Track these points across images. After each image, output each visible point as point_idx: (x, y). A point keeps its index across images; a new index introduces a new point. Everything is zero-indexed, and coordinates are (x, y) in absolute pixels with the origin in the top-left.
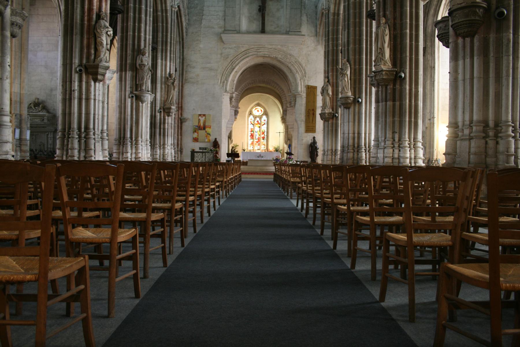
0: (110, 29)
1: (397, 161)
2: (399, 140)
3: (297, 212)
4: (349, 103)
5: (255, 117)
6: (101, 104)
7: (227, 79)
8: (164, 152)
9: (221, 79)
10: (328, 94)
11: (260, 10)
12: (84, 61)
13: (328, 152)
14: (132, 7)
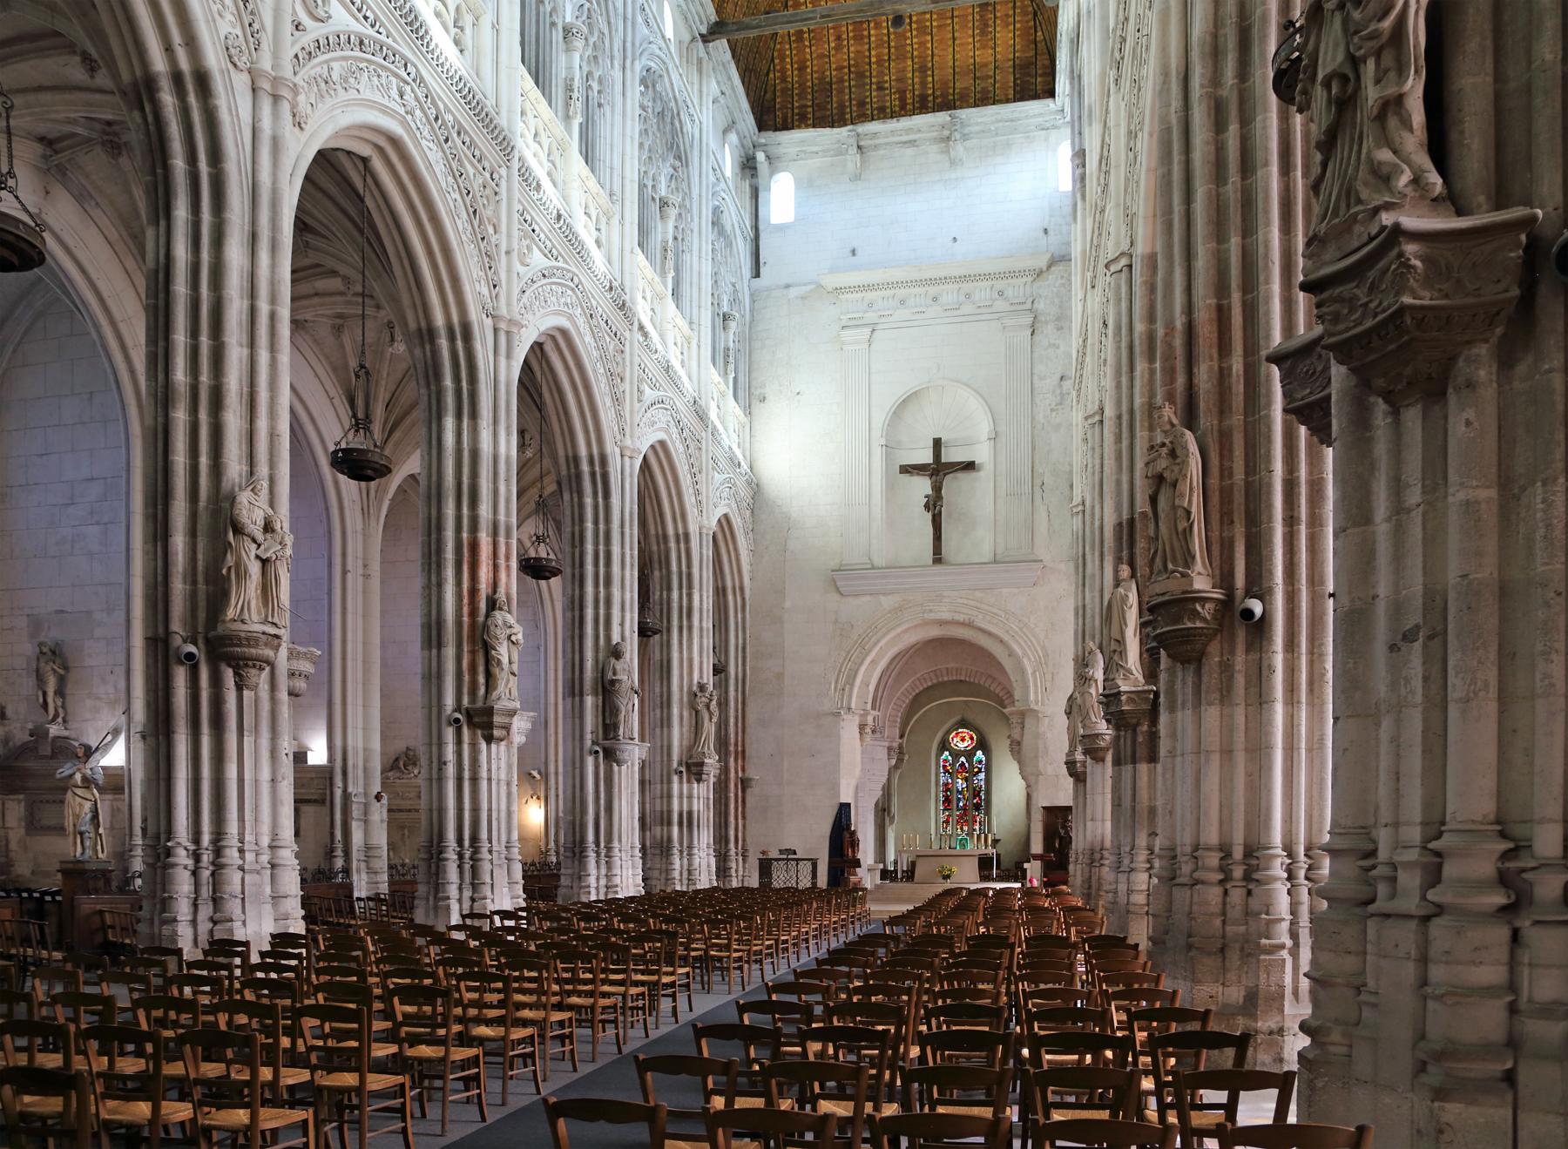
6: (504, 788)
7: (851, 681)
8: (690, 865)
11: (927, 507)
12: (465, 701)
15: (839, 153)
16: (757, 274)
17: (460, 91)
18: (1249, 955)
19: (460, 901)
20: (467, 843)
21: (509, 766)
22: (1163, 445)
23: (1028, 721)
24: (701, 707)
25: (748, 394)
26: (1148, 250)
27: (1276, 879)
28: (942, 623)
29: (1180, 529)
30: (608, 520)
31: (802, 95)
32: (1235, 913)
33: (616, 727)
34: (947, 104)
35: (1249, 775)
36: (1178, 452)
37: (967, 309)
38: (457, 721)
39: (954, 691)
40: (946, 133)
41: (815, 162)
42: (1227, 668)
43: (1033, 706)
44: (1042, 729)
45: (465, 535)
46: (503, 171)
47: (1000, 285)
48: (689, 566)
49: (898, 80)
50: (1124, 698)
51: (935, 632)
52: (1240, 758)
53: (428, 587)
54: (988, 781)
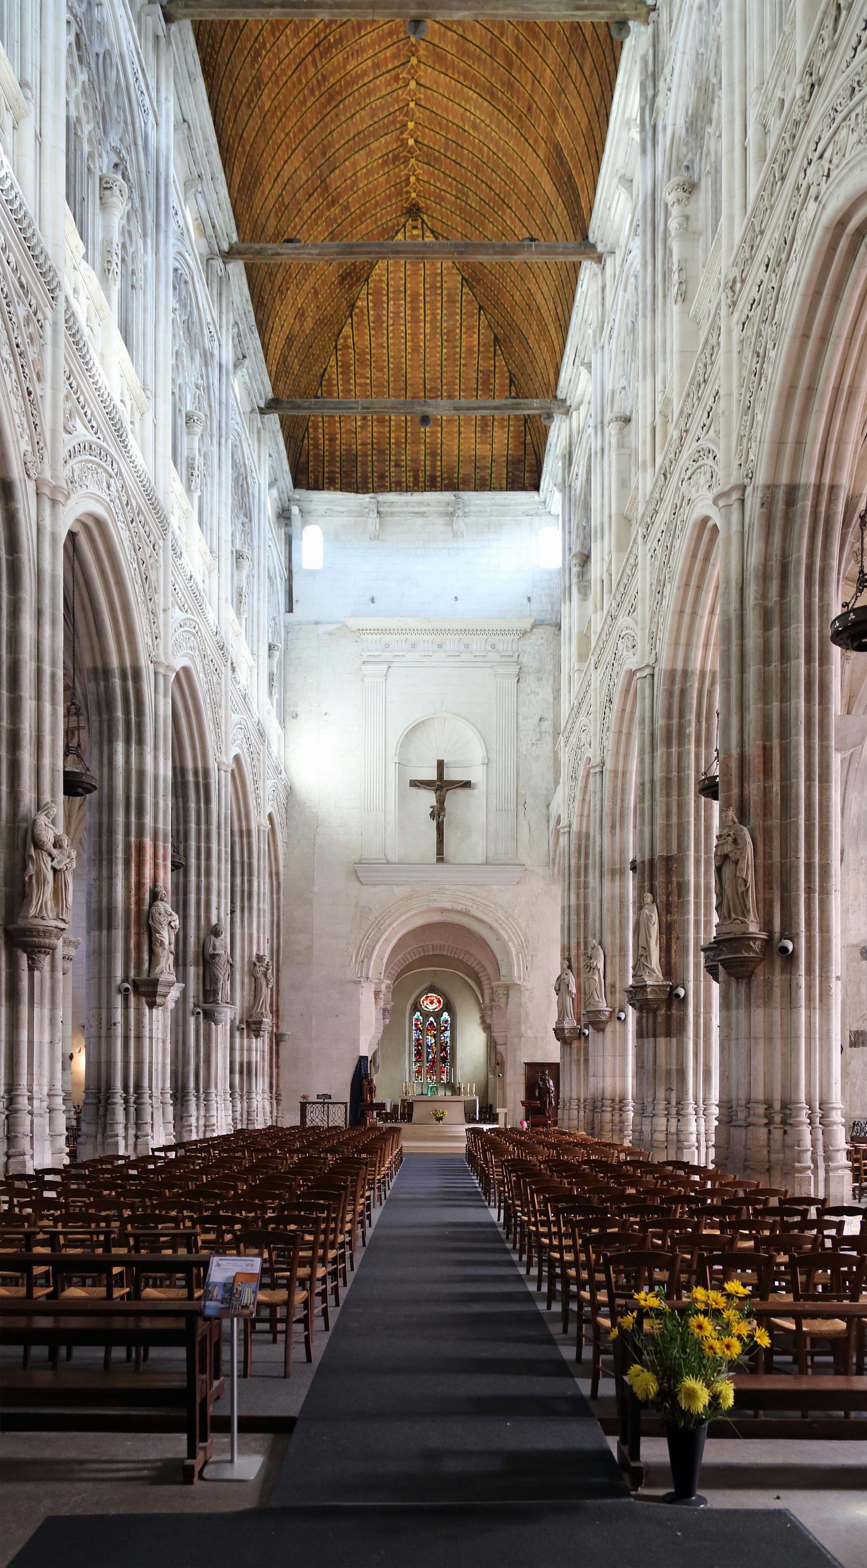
0: (176, 917)
1: (675, 1137)
2: (678, 1103)
3: (494, 1229)
4: (603, 1022)
6: (160, 1045)
7: (369, 956)
8: (249, 1107)
9: (357, 956)
10: (570, 993)
11: (432, 815)
15: (361, 515)
16: (290, 610)
17: (141, 482)
18: (787, 1174)
19: (126, 1138)
20: (131, 1090)
21: (165, 1027)
22: (729, 835)
23: (512, 994)
24: (259, 975)
25: (286, 714)
26: (669, 668)
27: (802, 1123)
28: (443, 910)
29: (740, 891)
30: (208, 822)
31: (331, 462)
32: (777, 1144)
34: (452, 486)
35: (783, 1054)
36: (739, 841)
37: (466, 657)
38: (127, 990)
39: (448, 963)
40: (451, 509)
41: (341, 520)
42: (768, 984)
44: (523, 1000)
45: (133, 839)
46: (161, 542)
47: (493, 639)
48: (250, 857)
49: (413, 461)
50: (649, 990)
51: (437, 918)
52: (778, 1043)
53: (99, 878)
54: (453, 1038)
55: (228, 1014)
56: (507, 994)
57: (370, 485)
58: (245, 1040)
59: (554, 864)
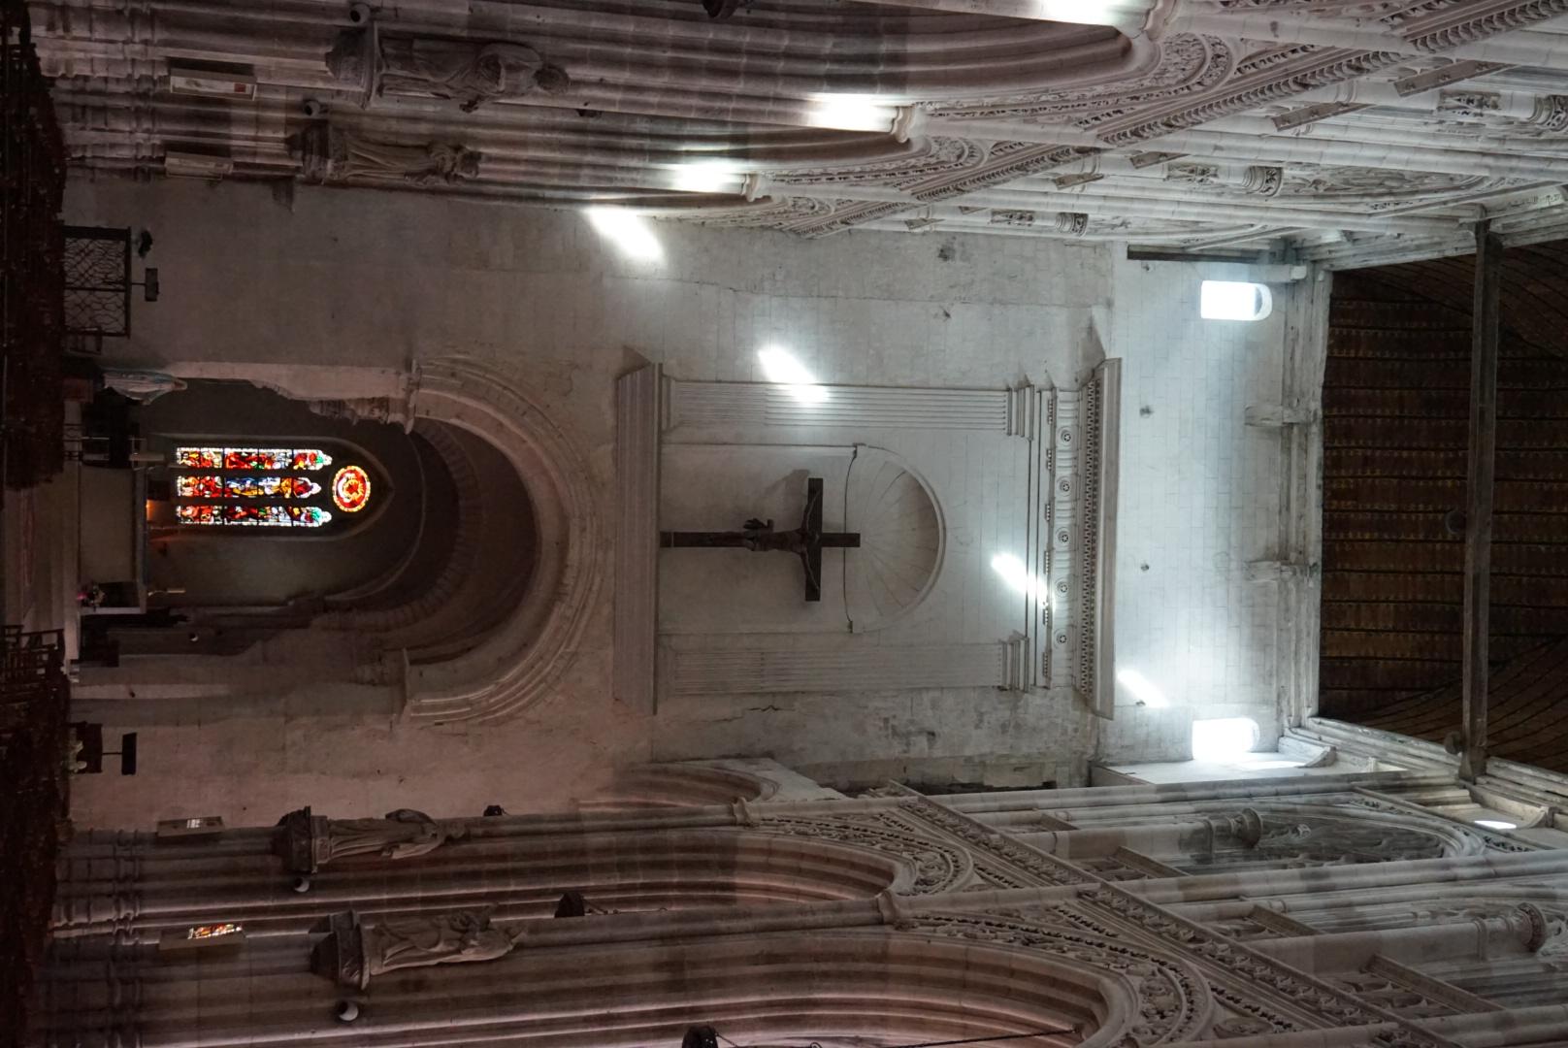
4: (335, 970)
5: (325, 477)
7: (467, 388)
8: (117, 112)
9: (466, 363)
10: (393, 845)
11: (754, 524)
13: (131, 859)
14: (740, 39)
16: (1132, 255)
27: (119, 910)
28: (563, 546)
33: (406, 61)
40: (1293, 556)
43: (411, 703)
51: (548, 531)
55: (348, 90)
56: (384, 684)
57: (1335, 412)
58: (281, 115)
59: (655, 772)
